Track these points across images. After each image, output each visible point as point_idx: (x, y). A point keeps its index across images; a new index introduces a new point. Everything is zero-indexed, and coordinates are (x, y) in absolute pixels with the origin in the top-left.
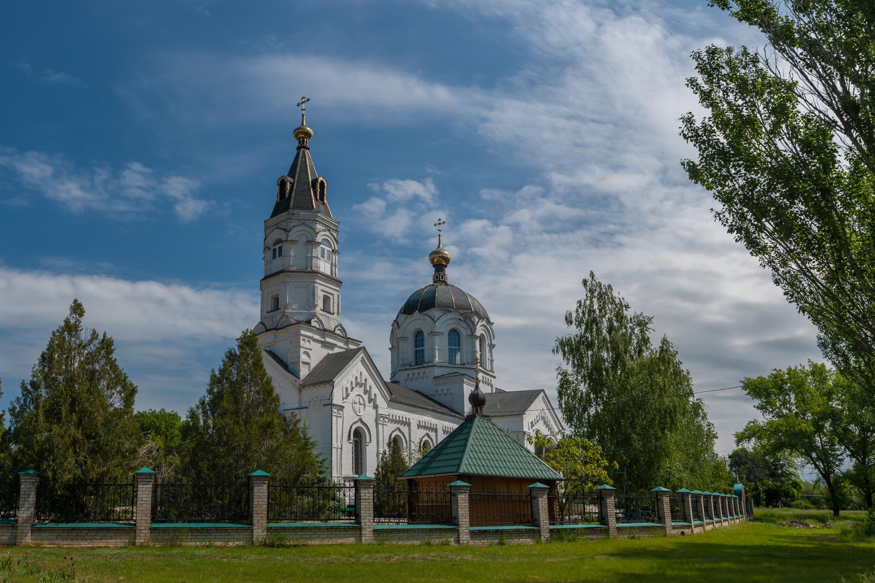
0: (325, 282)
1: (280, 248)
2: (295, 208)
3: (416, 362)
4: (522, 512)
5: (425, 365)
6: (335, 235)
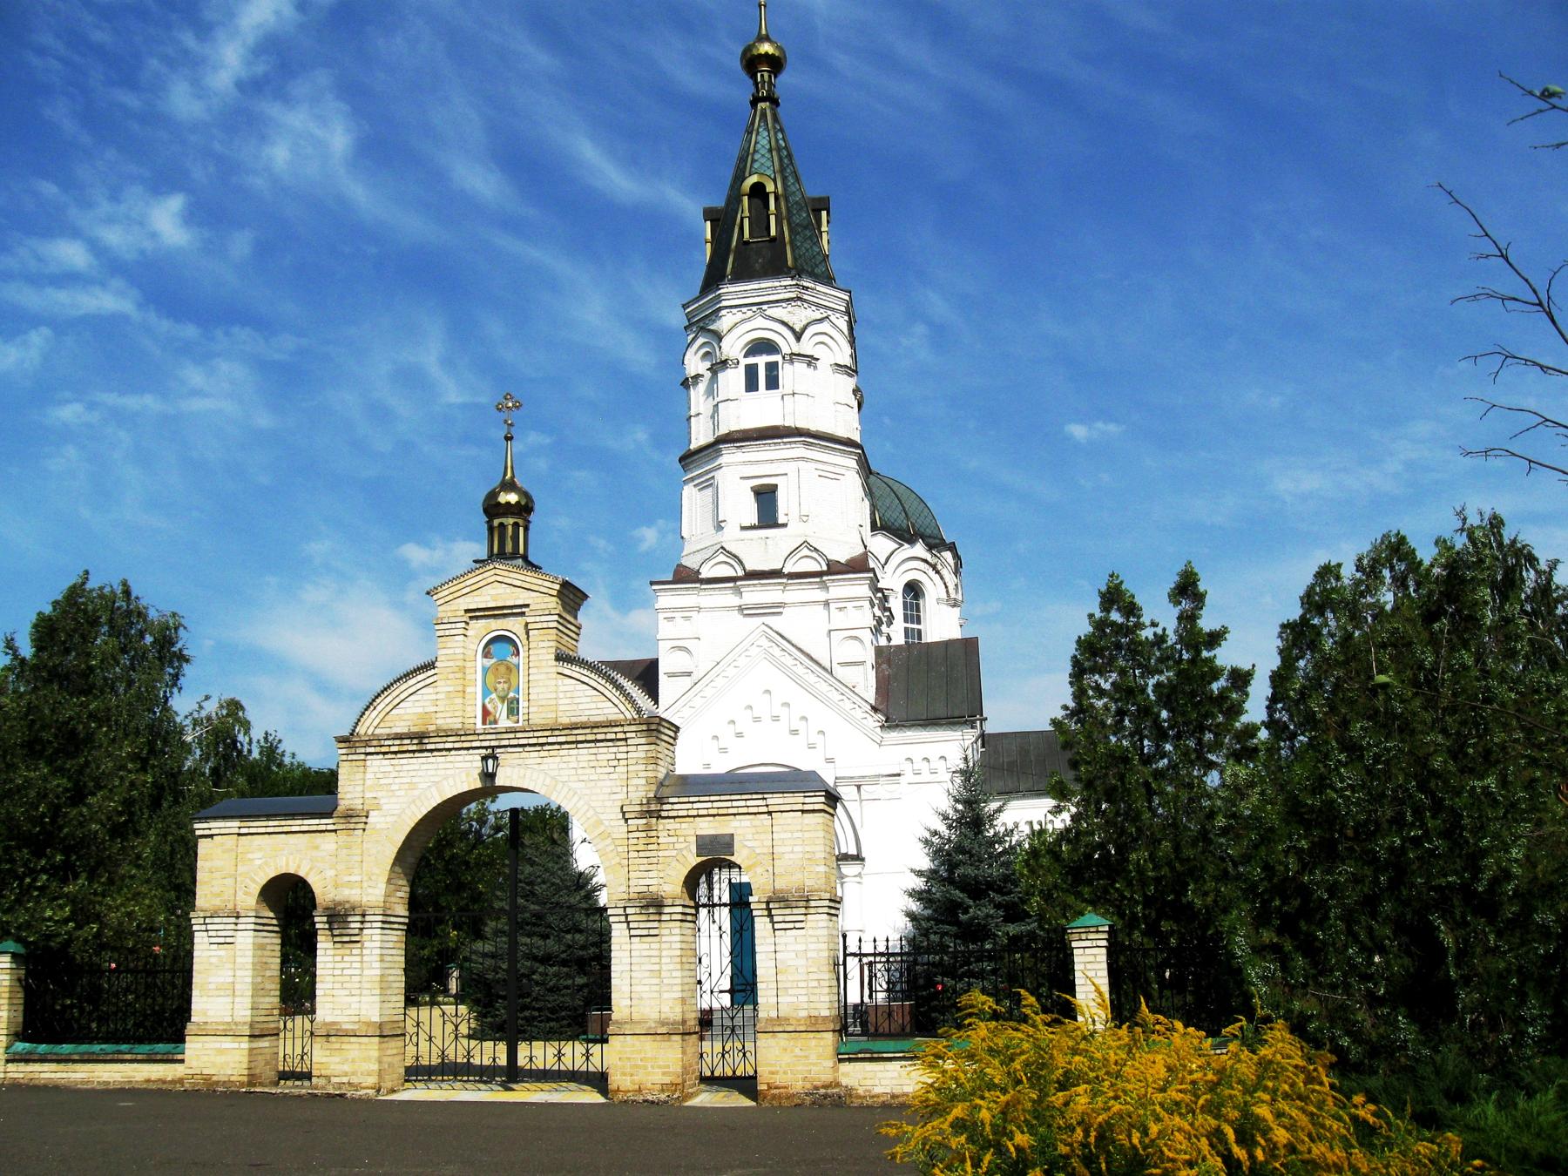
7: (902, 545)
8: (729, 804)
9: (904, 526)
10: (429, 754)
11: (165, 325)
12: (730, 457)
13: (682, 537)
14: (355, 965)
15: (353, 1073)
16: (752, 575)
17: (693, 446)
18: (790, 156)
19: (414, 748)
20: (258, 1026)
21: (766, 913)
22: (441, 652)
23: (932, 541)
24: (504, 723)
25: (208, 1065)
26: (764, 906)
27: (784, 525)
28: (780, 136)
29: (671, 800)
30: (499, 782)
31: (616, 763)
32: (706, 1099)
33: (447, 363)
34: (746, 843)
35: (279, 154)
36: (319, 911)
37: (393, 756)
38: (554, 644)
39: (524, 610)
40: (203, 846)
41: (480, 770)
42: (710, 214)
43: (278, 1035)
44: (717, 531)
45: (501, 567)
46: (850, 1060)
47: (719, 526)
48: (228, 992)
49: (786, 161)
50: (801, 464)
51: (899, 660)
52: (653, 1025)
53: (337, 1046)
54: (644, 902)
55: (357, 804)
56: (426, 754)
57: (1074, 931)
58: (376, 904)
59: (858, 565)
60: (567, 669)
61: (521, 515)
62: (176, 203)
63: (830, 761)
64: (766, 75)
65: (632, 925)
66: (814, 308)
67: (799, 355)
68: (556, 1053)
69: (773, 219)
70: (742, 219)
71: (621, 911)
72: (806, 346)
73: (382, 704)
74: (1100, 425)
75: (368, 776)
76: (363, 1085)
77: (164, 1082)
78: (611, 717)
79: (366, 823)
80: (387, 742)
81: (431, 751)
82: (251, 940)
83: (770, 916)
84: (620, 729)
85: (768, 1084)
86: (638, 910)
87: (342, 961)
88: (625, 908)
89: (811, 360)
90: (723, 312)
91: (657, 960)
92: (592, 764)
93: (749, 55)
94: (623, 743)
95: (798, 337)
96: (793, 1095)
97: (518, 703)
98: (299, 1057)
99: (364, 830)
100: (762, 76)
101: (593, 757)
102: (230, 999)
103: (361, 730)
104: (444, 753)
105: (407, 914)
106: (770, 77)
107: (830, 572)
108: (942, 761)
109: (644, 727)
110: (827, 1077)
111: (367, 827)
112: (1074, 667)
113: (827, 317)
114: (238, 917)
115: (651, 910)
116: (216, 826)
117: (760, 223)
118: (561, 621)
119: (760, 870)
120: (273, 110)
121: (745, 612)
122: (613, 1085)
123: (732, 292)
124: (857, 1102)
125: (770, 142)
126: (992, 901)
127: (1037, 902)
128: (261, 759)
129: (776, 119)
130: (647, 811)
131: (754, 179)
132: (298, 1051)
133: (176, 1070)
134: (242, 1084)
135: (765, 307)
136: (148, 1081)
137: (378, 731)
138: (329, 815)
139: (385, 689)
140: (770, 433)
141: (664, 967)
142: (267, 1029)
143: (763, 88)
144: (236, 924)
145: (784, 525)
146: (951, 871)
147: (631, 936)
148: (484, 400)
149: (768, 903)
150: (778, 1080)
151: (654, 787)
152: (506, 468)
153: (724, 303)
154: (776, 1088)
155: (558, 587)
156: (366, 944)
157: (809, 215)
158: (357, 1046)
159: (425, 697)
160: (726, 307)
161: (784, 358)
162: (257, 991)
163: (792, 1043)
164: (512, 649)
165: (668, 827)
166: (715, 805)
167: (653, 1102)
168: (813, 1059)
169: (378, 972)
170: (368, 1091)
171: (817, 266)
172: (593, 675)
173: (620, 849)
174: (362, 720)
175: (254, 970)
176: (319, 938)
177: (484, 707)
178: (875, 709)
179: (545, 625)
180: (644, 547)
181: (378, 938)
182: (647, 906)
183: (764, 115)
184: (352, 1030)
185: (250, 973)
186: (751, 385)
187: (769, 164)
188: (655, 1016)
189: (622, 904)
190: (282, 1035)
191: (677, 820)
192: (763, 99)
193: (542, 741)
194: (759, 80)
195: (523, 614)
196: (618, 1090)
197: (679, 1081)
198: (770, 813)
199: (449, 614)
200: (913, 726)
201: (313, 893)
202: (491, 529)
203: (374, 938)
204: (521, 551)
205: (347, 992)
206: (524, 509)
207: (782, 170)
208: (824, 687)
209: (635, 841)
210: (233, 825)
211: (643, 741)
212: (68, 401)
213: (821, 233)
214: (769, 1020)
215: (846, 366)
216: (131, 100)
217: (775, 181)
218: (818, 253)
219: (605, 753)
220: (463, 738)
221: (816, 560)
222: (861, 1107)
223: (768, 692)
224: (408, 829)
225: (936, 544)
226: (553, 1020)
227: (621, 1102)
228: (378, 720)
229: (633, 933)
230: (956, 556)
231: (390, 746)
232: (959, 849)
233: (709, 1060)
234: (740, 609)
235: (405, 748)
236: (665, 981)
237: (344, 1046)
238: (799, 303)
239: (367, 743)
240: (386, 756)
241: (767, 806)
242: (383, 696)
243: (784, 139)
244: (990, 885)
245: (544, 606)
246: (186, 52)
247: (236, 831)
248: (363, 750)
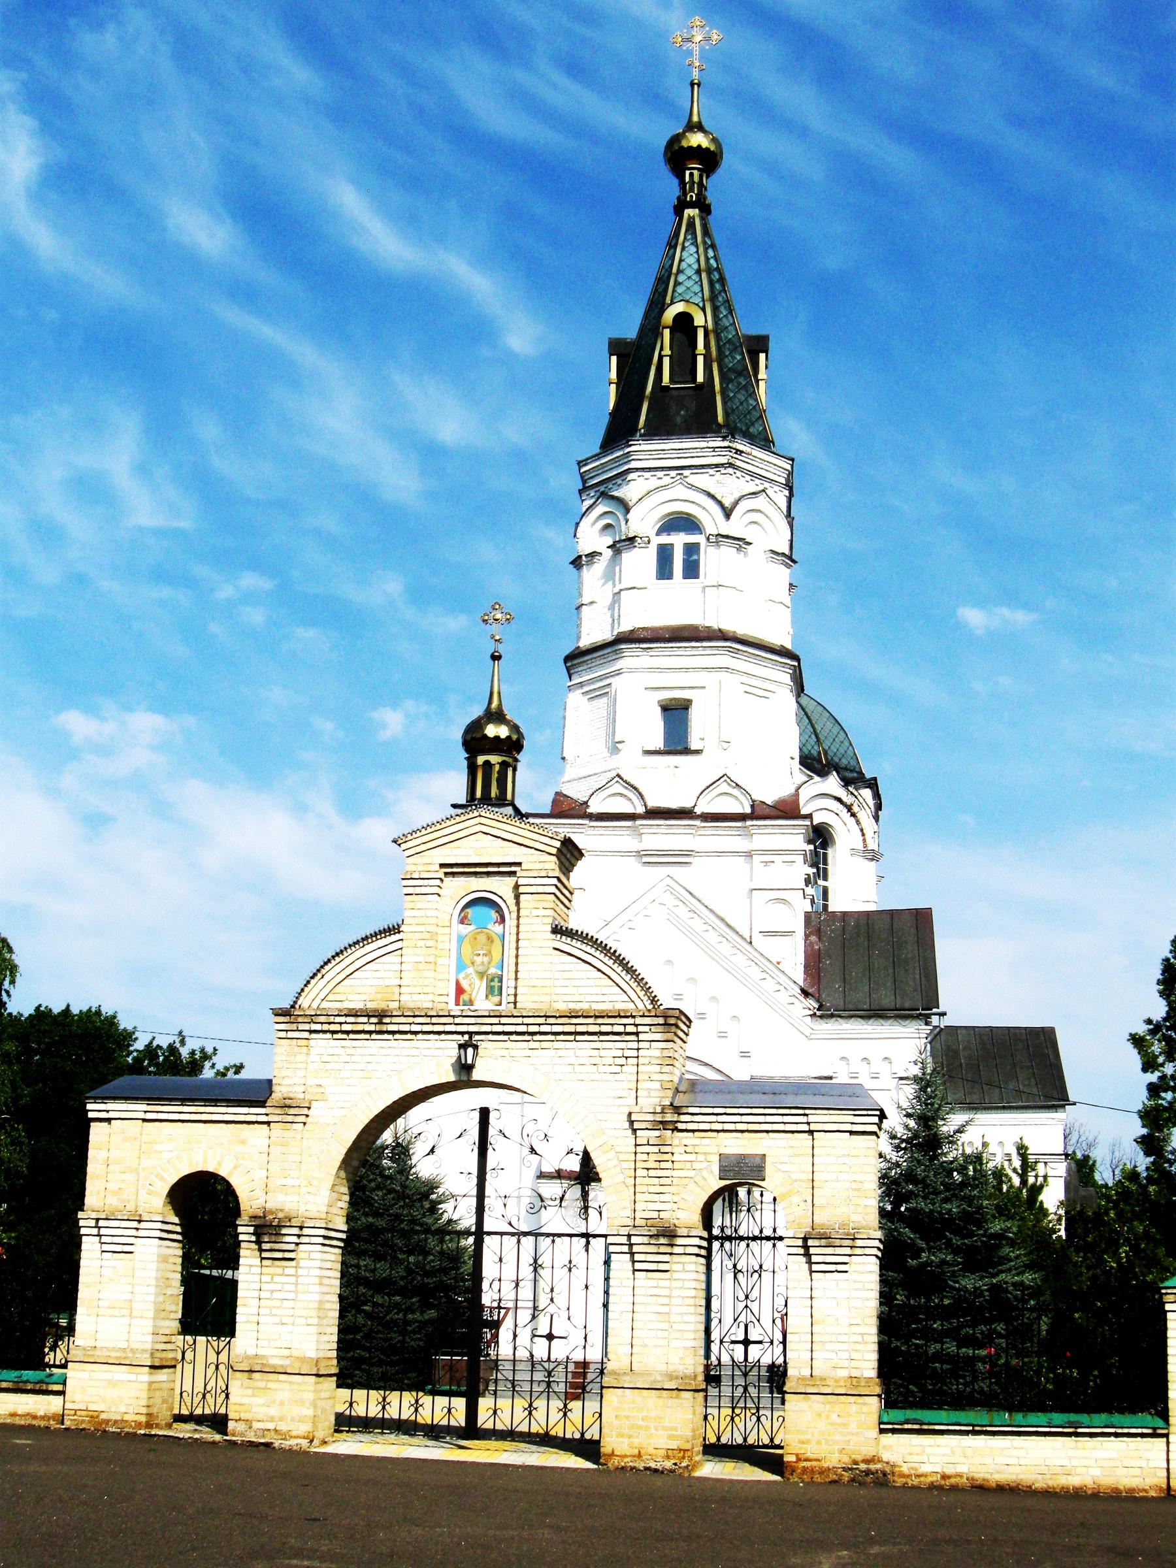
7: (811, 778)
8: (737, 1119)
9: (814, 753)
10: (390, 1037)
12: (633, 659)
13: (563, 758)
14: (287, 1287)
15: (282, 1419)
16: (655, 814)
17: (585, 642)
18: (722, 280)
19: (372, 1028)
20: (158, 1355)
21: (802, 1251)
22: (407, 913)
23: (849, 775)
24: (483, 1004)
25: (95, 1399)
26: (800, 1243)
27: (698, 752)
28: (711, 253)
29: (691, 1110)
30: (476, 1075)
31: (623, 1061)
32: (711, 1469)
33: (142, 470)
34: (780, 1166)
36: (243, 1219)
37: (344, 1036)
38: (551, 912)
39: (513, 869)
40: (97, 1132)
41: (453, 1060)
42: (617, 347)
43: (174, 1367)
44: (612, 754)
45: (487, 815)
46: (893, 1431)
47: (615, 747)
48: (124, 1312)
49: (718, 286)
50: (723, 675)
51: (832, 931)
52: (659, 1378)
53: (262, 1384)
54: (654, 1231)
55: (297, 1093)
56: (386, 1036)
57: (1169, 1291)
58: (317, 1215)
59: (787, 810)
60: (565, 943)
61: (510, 753)
63: (745, 1054)
64: (696, 173)
65: (104, 1239)
66: (748, 478)
67: (727, 537)
68: (527, 1406)
69: (700, 360)
70: (661, 357)
71: (624, 1240)
72: (733, 527)
73: (332, 972)
74: (1005, 612)
75: (312, 1058)
76: (294, 1433)
77: (35, 1417)
78: (620, 1006)
79: (307, 1116)
80: (338, 1019)
81: (393, 1033)
82: (155, 1250)
83: (807, 1255)
84: (630, 1021)
85: (797, 1455)
86: (645, 1240)
87: (272, 1282)
88: (629, 1236)
89: (741, 543)
90: (631, 476)
91: (666, 1301)
92: (594, 1061)
93: (676, 147)
94: (633, 1038)
95: (728, 513)
96: (828, 1470)
97: (501, 981)
98: (200, 1396)
99: (305, 1124)
100: (691, 175)
101: (596, 1053)
102: (127, 1320)
103: (304, 1002)
104: (409, 1036)
105: (345, 1228)
106: (701, 177)
107: (753, 816)
108: (843, 1063)
109: (661, 1020)
110: (868, 1451)
111: (308, 1120)
112: (1164, 972)
113: (763, 491)
114: (140, 1221)
115: (662, 1240)
116: (115, 1108)
117: (684, 363)
118: (559, 885)
119: (796, 1199)
121: (646, 859)
122: (606, 1449)
123: (644, 451)
124: (900, 1481)
125: (698, 261)
126: (949, 1244)
127: (1125, 1252)
128: (5, 1018)
129: (706, 232)
130: (661, 1122)
131: (679, 308)
132: (199, 1387)
133: (49, 1404)
134: (139, 1425)
135: (686, 472)
136: (13, 1415)
137: (325, 1005)
138: (262, 1104)
139: (337, 954)
140: (686, 634)
141: (675, 1310)
142: (167, 1360)
143: (692, 190)
144: (299, 1236)
145: (698, 752)
146: (896, 1205)
147: (635, 1270)
148: (185, 524)
149: (805, 1239)
150: (810, 1451)
151: (670, 1093)
152: (491, 694)
153: (633, 465)
154: (806, 1460)
155: (558, 844)
156: (302, 1263)
157: (744, 358)
158: (287, 1386)
159: (387, 967)
160: (637, 469)
161: (708, 539)
162: (160, 1313)
163: (828, 1407)
164: (494, 915)
165: (685, 1142)
166: (721, 1118)
167: (656, 1471)
168: (853, 1427)
169: (317, 1297)
170: (299, 1441)
171: (753, 424)
172: (597, 954)
173: (625, 1165)
174: (306, 990)
175: (157, 1286)
176: (243, 1252)
177: (458, 983)
178: (805, 993)
179: (541, 889)
180: (385, 735)
181: (319, 1256)
182: (657, 1236)
183: (691, 224)
184: (282, 1366)
185: (152, 1290)
186: (664, 570)
187: (697, 288)
188: (662, 1367)
189: (625, 1231)
190: (179, 1366)
191: (697, 1134)
192: (692, 205)
193: (532, 1029)
194: (687, 179)
195: (513, 873)
196: (613, 1454)
197: (688, 1446)
198: (811, 1132)
199: (421, 868)
200: (851, 1017)
201: (236, 1197)
202: (472, 769)
203: (313, 1255)
204: (509, 796)
205: (277, 1320)
206: (512, 746)
207: (713, 298)
208: (740, 960)
209: (645, 1157)
210: (139, 1108)
211: (658, 1037)
213: (757, 381)
214: (801, 1379)
215: (783, 554)
217: (704, 310)
218: (754, 407)
219: (611, 1049)
220: (434, 1020)
221: (736, 797)
222: (904, 1486)
223: (669, 962)
224: (361, 1127)
225: (853, 778)
226: (387, 1364)
227: (617, 1468)
228: (326, 991)
229: (105, 1247)
230: (877, 796)
231: (341, 1023)
232: (909, 1176)
233: (715, 1424)
234: (639, 854)
235: (360, 1027)
236: (675, 1326)
237: (270, 1385)
238: (730, 470)
239: (312, 1019)
240: (335, 1036)
241: (808, 1123)
242: (333, 963)
243: (716, 258)
244: (948, 1223)
245: (540, 866)
247: (142, 1115)
248: (307, 1027)
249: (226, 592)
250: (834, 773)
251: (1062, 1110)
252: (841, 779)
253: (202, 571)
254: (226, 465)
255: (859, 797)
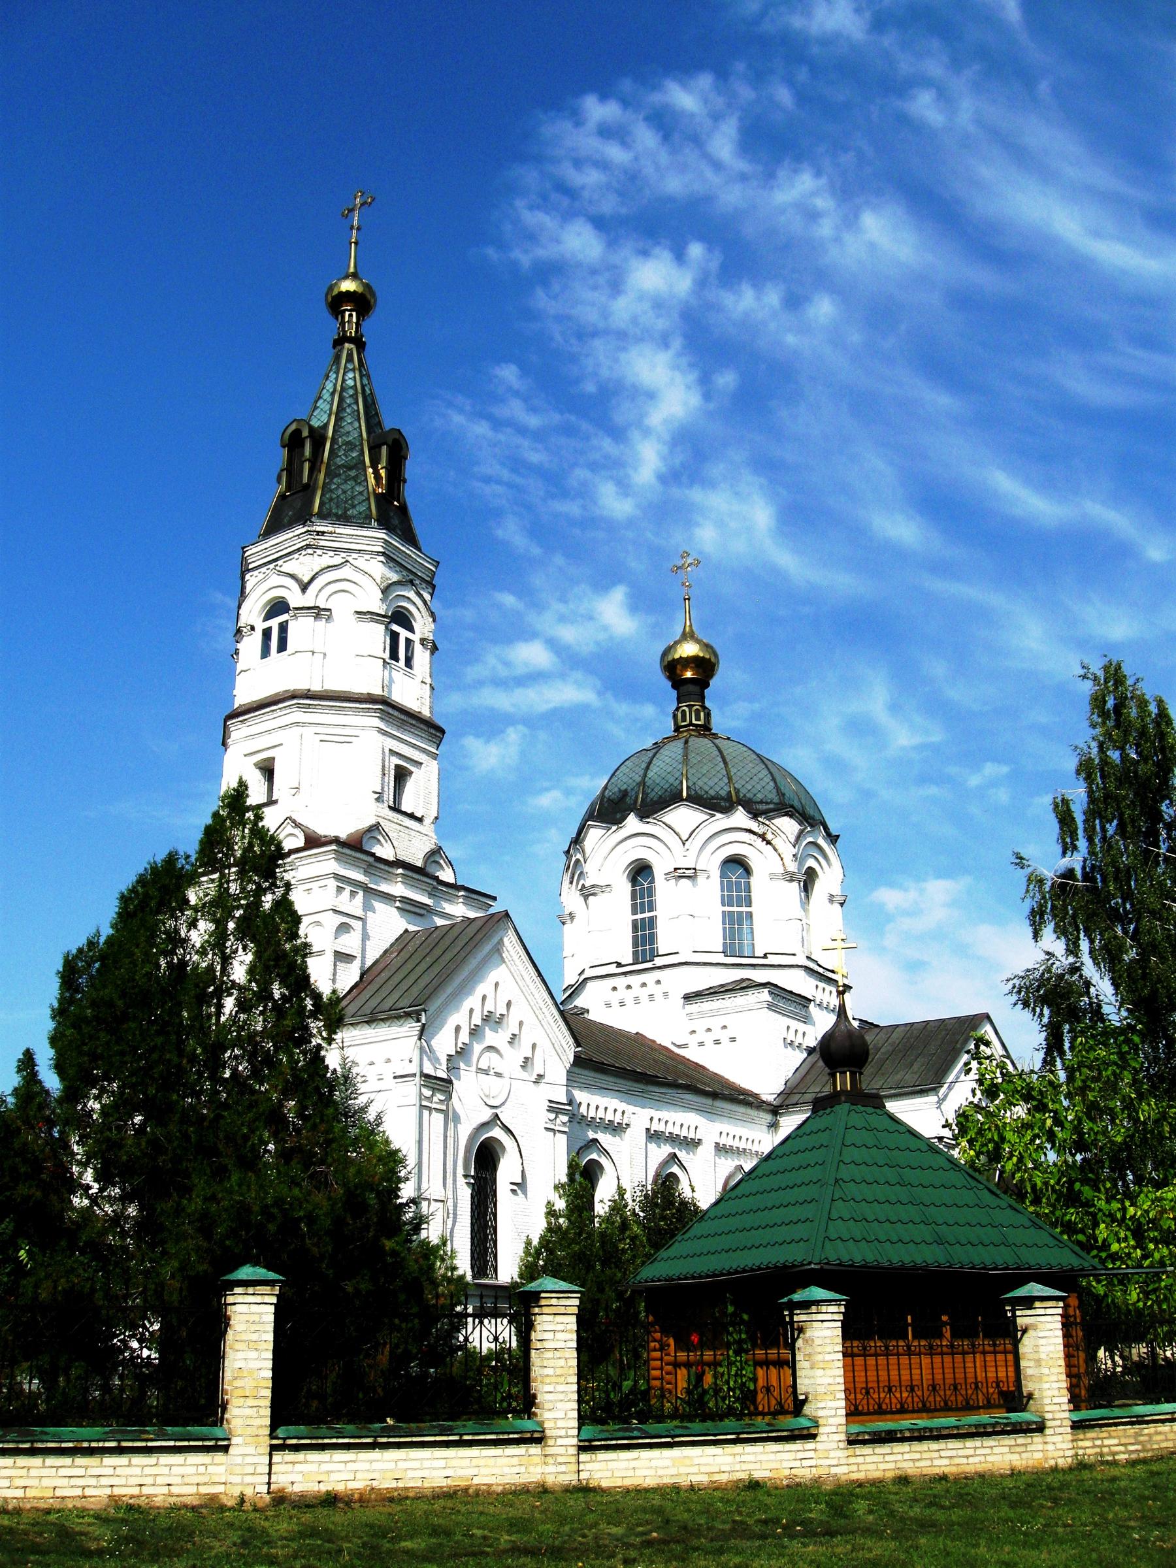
0: (399, 728)
1: (283, 628)
2: (323, 516)
3: (635, 953)
4: (992, 1375)
5: (659, 961)
6: (427, 597)
11: (622, 709)
33: (894, 708)
35: (706, 537)
62: (619, 594)
66: (332, 553)
89: (319, 612)
95: (304, 587)
120: (696, 495)
212: (547, 789)
216: (572, 508)
238: (310, 551)
246: (606, 457)
249: (974, 781)
250: (740, 807)
251: (934, 1093)
252: (749, 812)
253: (952, 770)
254: (958, 694)
255: (771, 825)
